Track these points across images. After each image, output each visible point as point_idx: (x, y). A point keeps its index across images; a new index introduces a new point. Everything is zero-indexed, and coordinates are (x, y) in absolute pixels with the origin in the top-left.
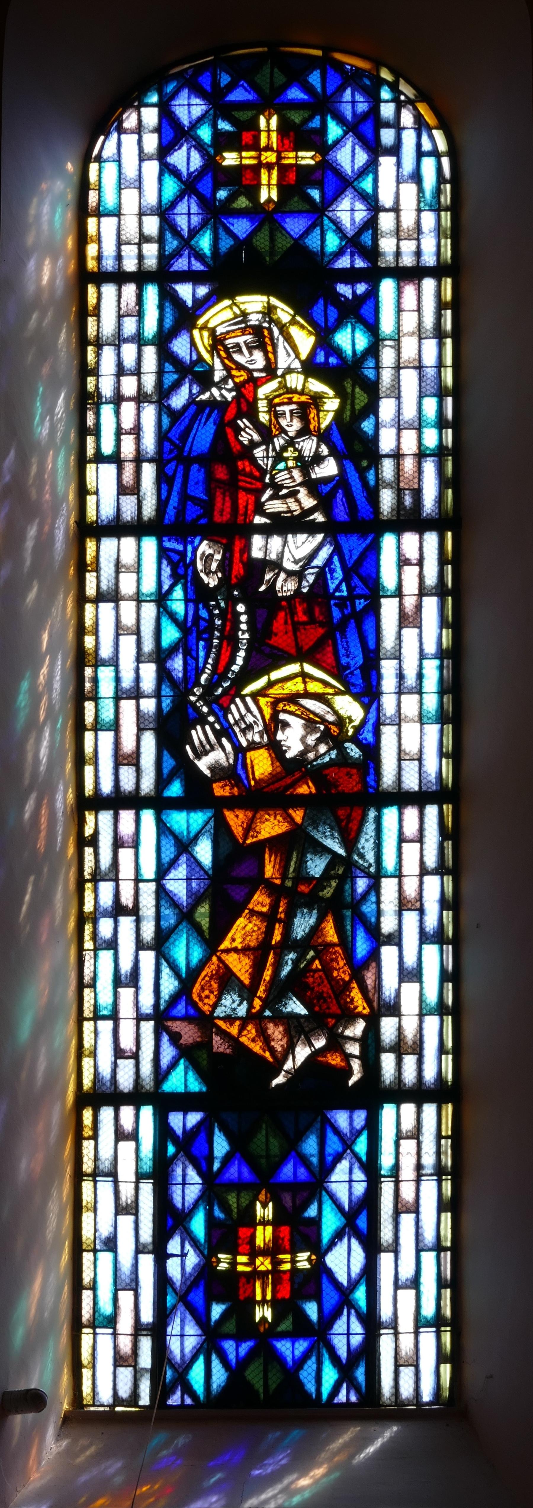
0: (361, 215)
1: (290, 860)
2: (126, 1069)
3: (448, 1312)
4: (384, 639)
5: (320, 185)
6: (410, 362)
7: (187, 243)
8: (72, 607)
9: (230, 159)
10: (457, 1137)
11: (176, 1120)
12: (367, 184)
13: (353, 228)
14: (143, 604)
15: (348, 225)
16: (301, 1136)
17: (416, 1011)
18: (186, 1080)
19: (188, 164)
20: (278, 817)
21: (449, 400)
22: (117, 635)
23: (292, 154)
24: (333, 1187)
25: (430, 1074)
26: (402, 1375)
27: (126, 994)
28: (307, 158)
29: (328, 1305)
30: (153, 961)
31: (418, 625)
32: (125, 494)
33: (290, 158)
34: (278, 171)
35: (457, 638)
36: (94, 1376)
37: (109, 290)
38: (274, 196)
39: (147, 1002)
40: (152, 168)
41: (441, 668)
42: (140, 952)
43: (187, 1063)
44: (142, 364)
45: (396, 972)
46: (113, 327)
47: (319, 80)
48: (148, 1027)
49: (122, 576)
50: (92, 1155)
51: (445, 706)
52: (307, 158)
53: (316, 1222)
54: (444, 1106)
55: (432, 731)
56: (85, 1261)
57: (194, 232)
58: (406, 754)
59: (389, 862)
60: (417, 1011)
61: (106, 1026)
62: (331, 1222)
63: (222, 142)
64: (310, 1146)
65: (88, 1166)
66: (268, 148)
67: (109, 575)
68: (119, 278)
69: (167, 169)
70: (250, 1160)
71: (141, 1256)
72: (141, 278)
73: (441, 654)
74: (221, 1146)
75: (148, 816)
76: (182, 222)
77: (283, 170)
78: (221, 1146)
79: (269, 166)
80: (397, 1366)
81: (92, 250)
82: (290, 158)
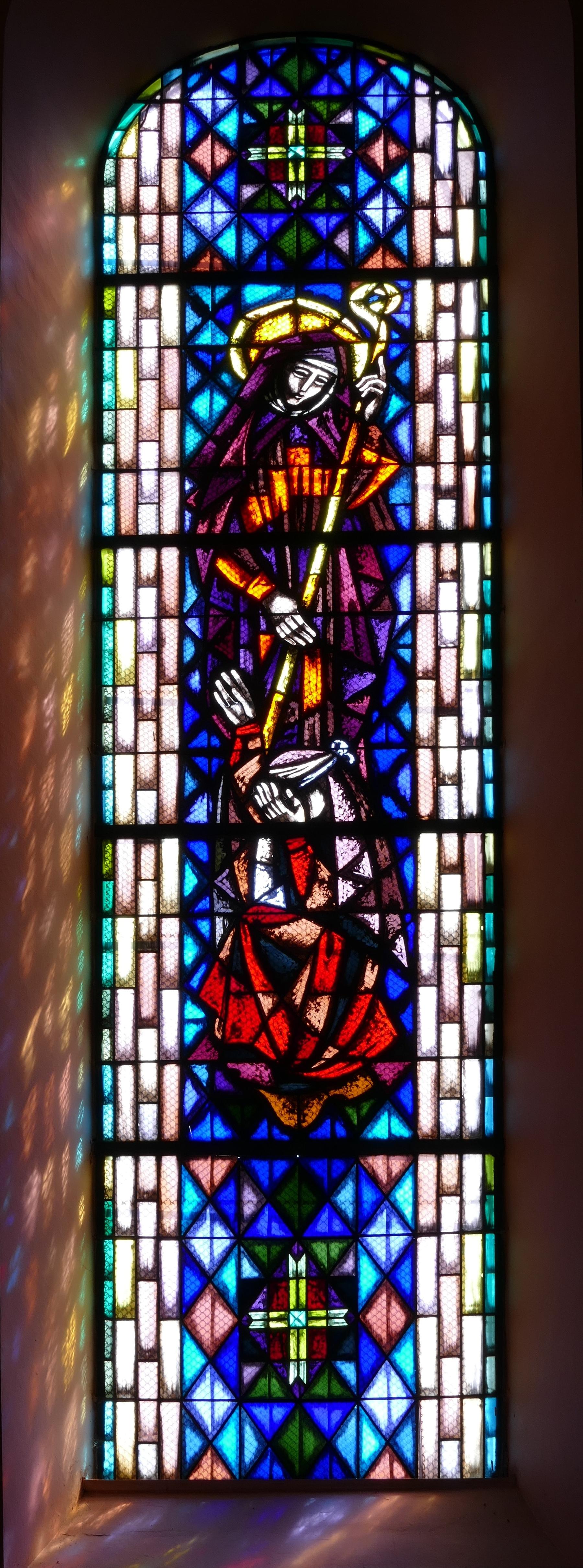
0: (398, 1243)
1: (321, 732)
2: (147, 799)
3: (486, 331)
4: (421, 373)
5: (354, 1357)
6: (452, 1269)
7: (209, 1444)
8: (86, 1339)
9: (255, 154)
10: (499, 780)
11: (201, 1167)
12: (400, 181)
13: (389, 1263)
14: (164, 920)
15: (384, 1259)
16: (336, 1186)
17: (453, 336)
18: (213, 1315)
19: (212, 1328)
20: (308, 938)
21: (487, 468)
22: (138, 319)
23: (321, 149)
24: (370, 1404)
25: (472, 1123)
26: (444, 1206)
27: (148, 1036)
28: (339, 1317)
29: (366, 1367)
30: (175, 227)
31: (459, 1096)
32: (145, 1360)
33: (319, 153)
34: (305, 166)
35: (497, 658)
36: (115, 961)
37: (126, 555)
38: (303, 1376)
39: (171, 1040)
40: (171, 418)
41: (483, 993)
42: (162, 1322)
43: (213, 1370)
44: (161, 779)
45: (435, 865)
46: (129, 811)
47: (349, 72)
48: (172, 1072)
49: (143, 190)
50: (111, 804)
51: (487, 1218)
52: (339, 1317)
53: (353, 1279)
54: (487, 835)
55: (474, 1242)
56: (105, 420)
57: (218, 116)
58: (445, 939)
59: (426, 966)
60: (453, 337)
61: (127, 480)
62: (368, 1278)
63: (247, 138)
64: (345, 1197)
65: (107, 904)
66: (297, 143)
67: (126, 1045)
68: (137, 542)
69: (187, 416)
70: (280, 1215)
71: (164, 1323)
72: (158, 279)
73: (480, 397)
74: (250, 1201)
75: (170, 1163)
76: (203, 1410)
77: (311, 164)
78: (250, 1201)
79: (296, 160)
80: (439, 946)
81: (108, 251)
82: (319, 153)
